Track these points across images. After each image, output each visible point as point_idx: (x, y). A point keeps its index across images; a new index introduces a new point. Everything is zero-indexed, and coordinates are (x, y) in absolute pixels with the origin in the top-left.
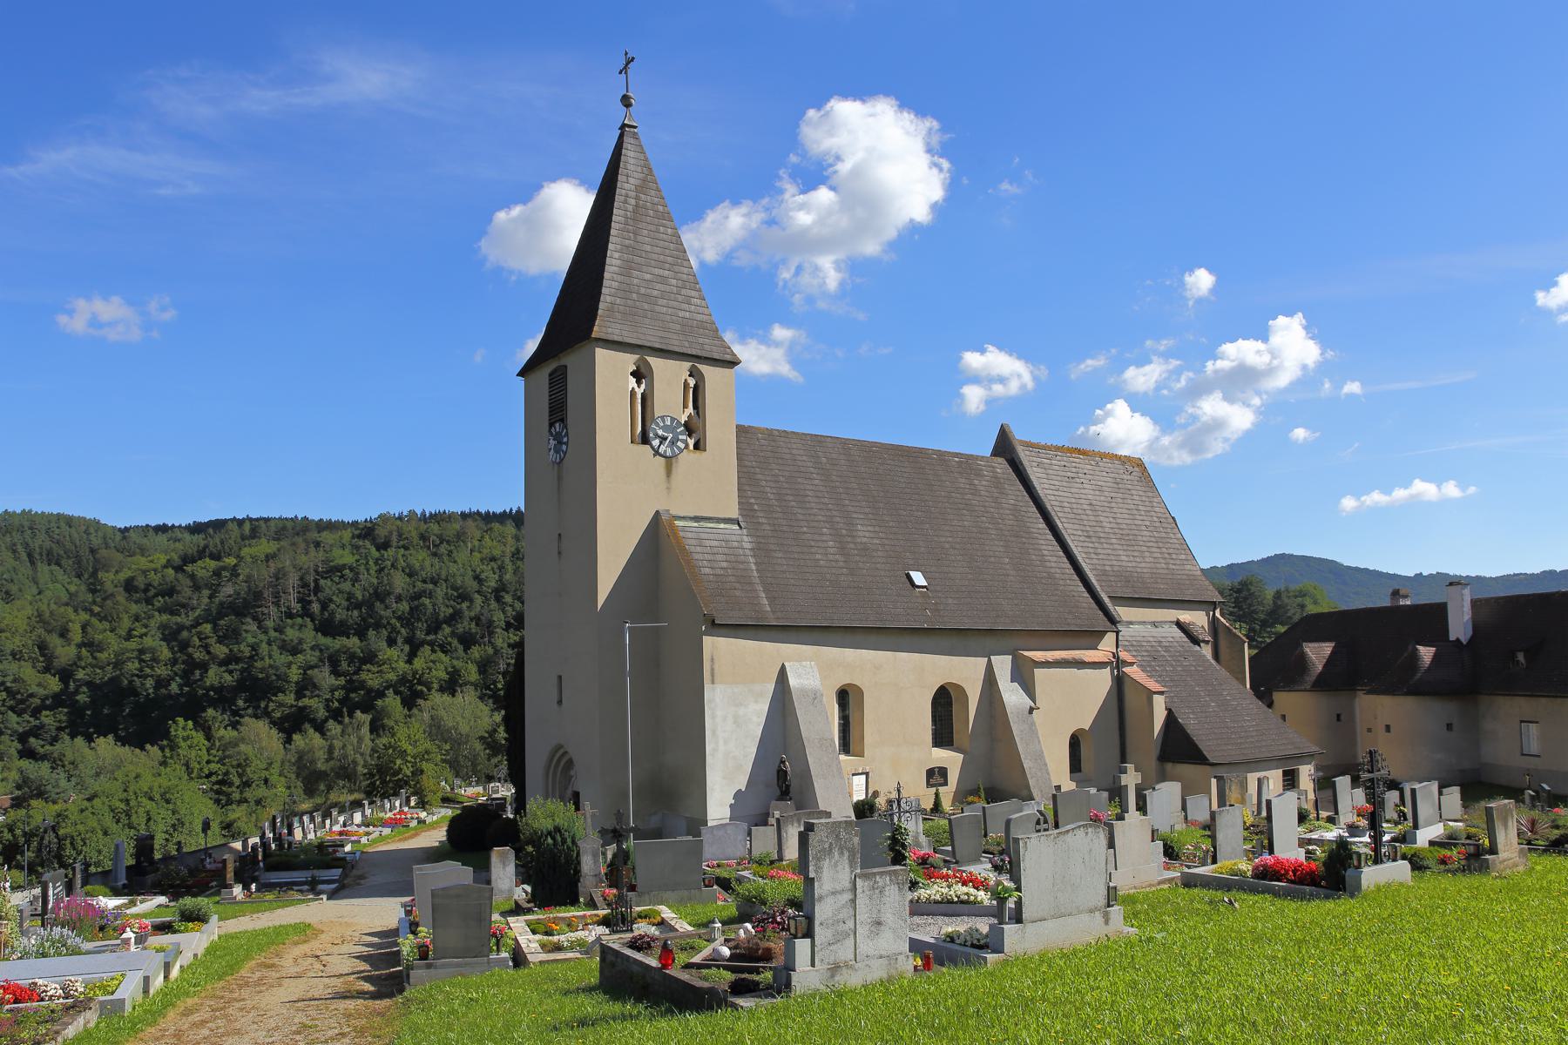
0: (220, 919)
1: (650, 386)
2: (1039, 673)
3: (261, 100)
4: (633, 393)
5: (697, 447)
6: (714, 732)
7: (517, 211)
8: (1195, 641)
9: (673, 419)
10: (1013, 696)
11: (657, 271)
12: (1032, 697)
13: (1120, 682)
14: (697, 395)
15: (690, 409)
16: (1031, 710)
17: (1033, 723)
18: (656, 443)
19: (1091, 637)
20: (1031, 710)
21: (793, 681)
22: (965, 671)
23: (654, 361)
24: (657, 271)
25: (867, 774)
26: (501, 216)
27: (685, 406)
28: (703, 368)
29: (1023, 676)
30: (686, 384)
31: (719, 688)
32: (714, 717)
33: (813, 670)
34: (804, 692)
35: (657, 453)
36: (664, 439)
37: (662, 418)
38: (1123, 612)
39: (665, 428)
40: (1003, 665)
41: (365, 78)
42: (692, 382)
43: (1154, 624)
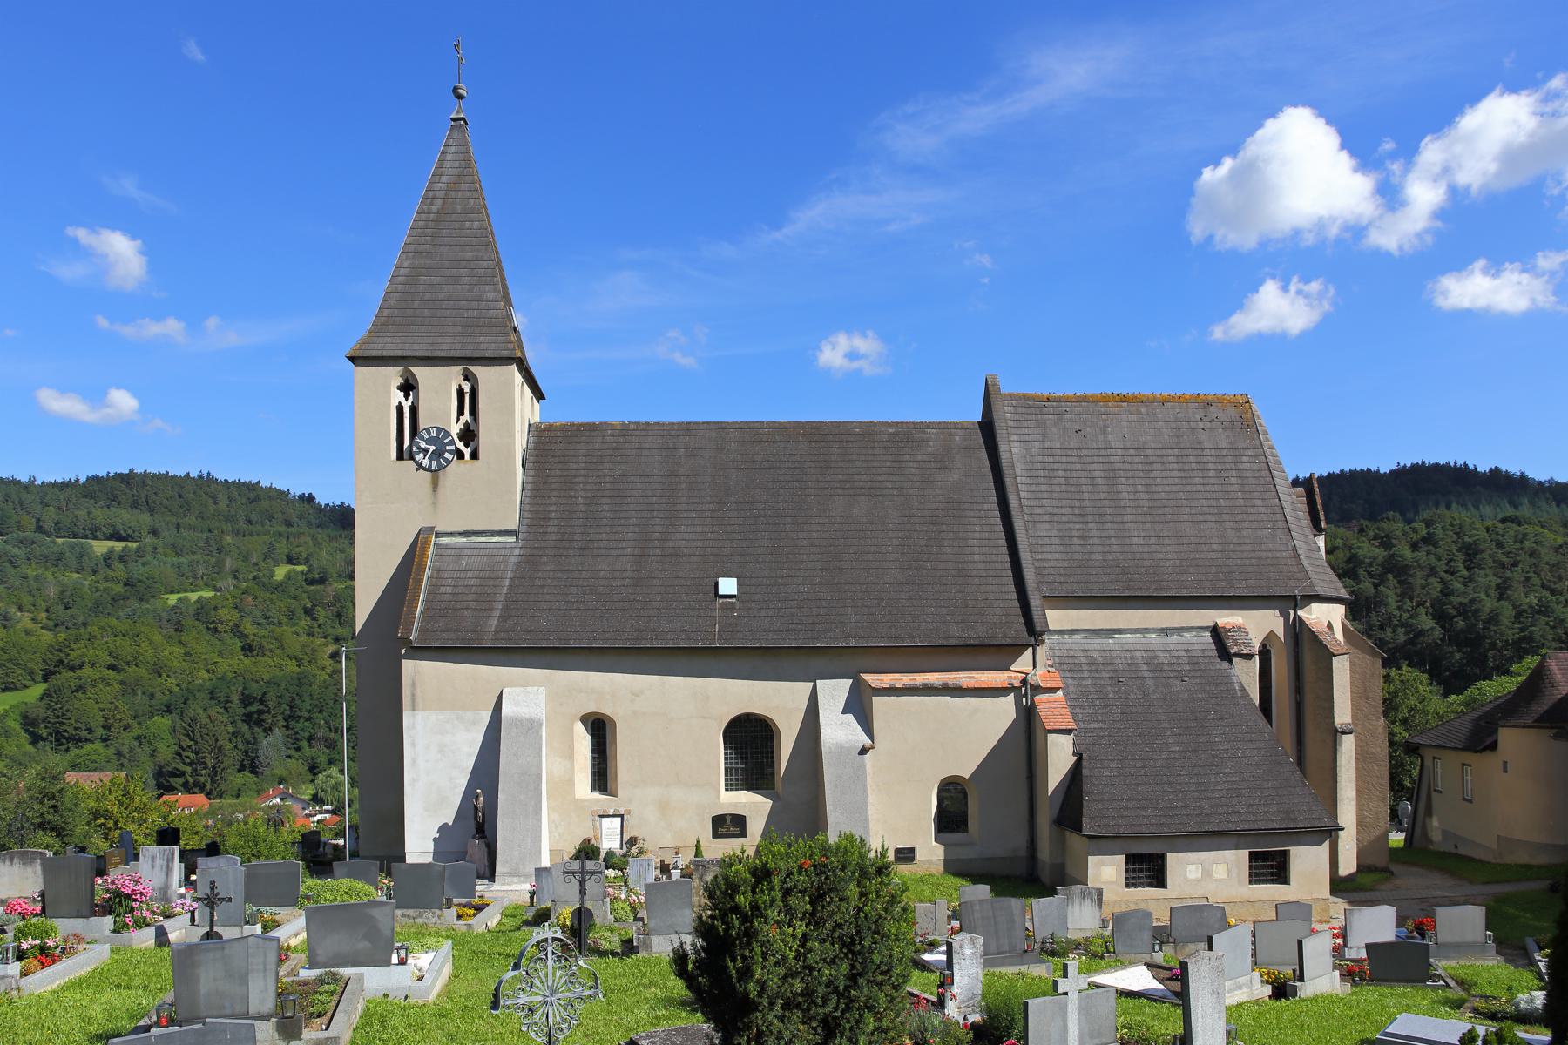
0: (491, 876)
1: (416, 398)
2: (877, 701)
3: (975, 117)
4: (400, 408)
5: (474, 456)
6: (414, 761)
7: (1228, 163)
8: (1225, 655)
9: (439, 429)
10: (838, 730)
11: (448, 272)
12: (869, 732)
13: (1028, 718)
14: (469, 400)
15: (466, 416)
16: (864, 751)
17: (862, 767)
18: (419, 457)
19: (1003, 655)
20: (864, 751)
21: (506, 710)
22: (779, 700)
23: (419, 372)
24: (448, 272)
25: (622, 816)
26: (1208, 175)
27: (461, 412)
28: (477, 370)
29: (859, 707)
30: (461, 392)
31: (420, 715)
32: (413, 745)
33: (537, 697)
34: (518, 722)
35: (420, 466)
36: (426, 451)
37: (428, 430)
38: (1056, 618)
39: (427, 442)
40: (834, 692)
41: (1070, 71)
42: (467, 387)
43: (1165, 631)
